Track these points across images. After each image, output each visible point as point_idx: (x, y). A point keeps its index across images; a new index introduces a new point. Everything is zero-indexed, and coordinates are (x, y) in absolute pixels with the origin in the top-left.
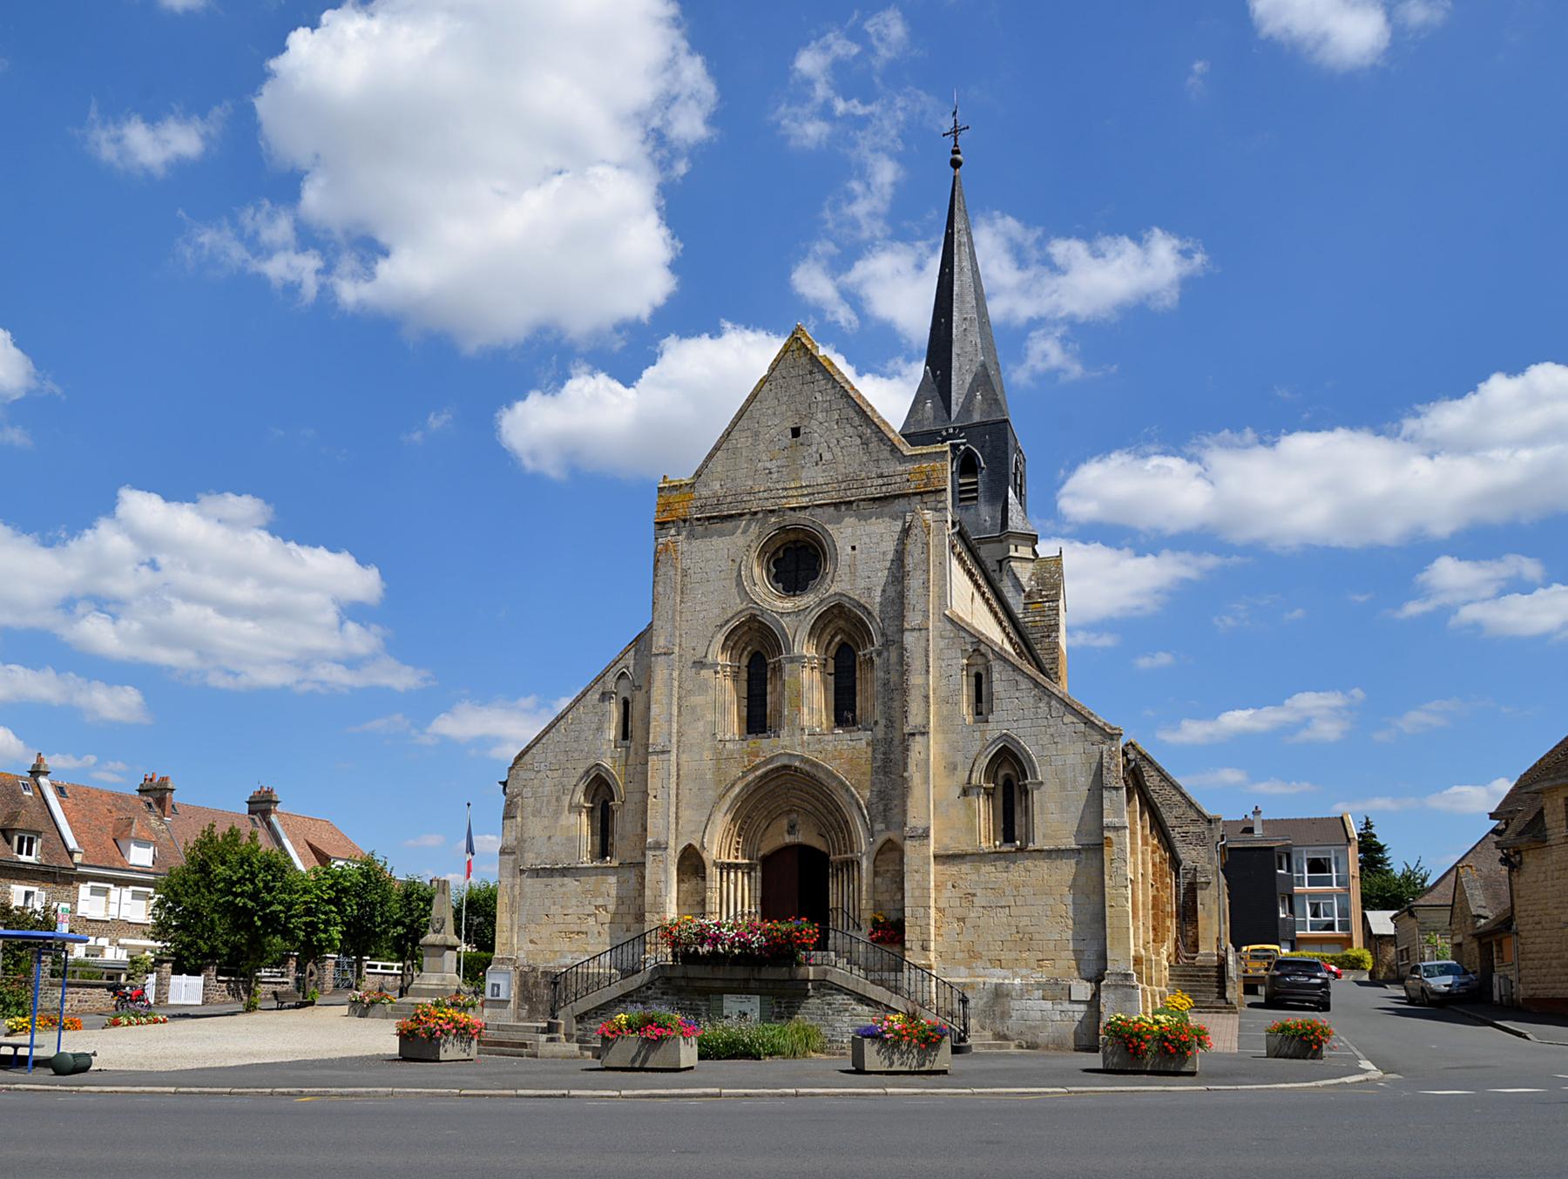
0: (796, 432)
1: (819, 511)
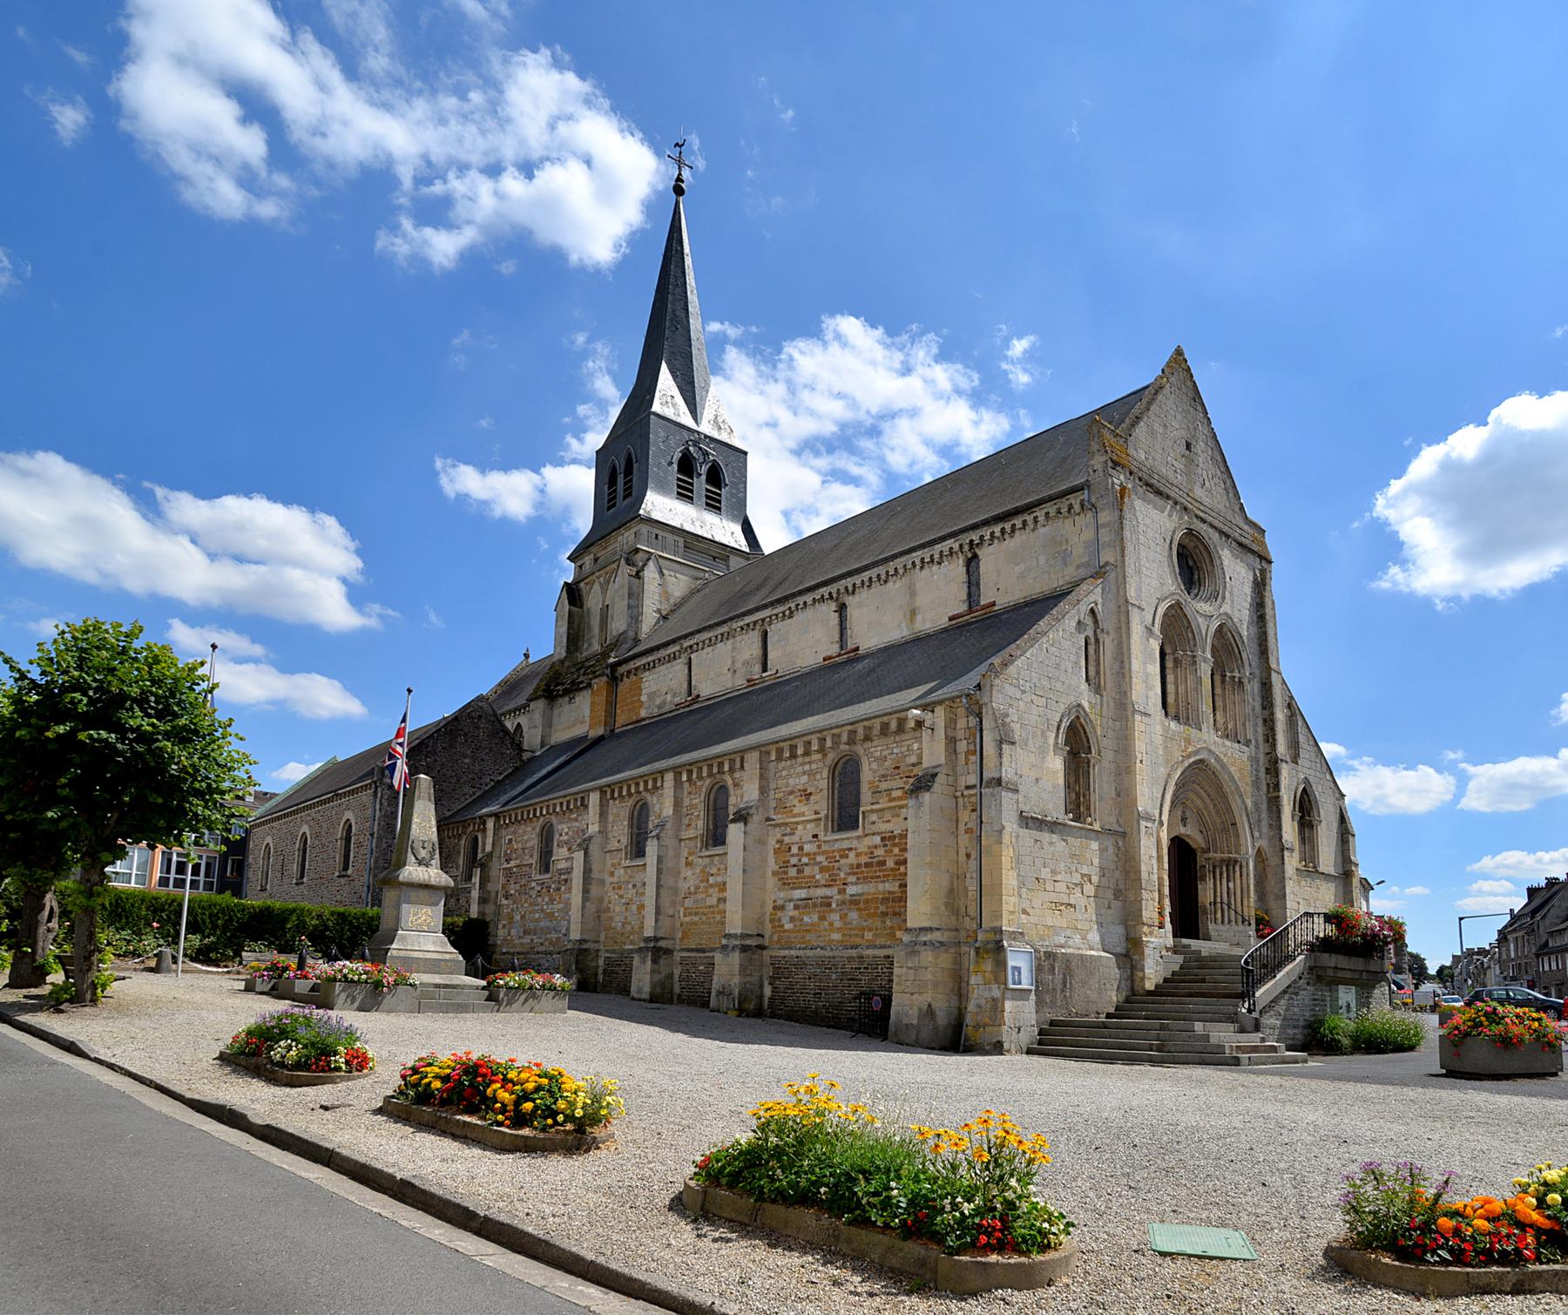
0: (1188, 446)
1: (1211, 531)
